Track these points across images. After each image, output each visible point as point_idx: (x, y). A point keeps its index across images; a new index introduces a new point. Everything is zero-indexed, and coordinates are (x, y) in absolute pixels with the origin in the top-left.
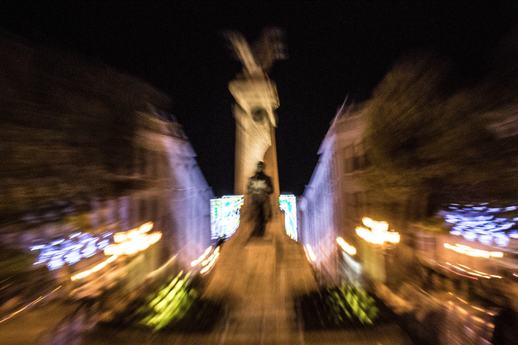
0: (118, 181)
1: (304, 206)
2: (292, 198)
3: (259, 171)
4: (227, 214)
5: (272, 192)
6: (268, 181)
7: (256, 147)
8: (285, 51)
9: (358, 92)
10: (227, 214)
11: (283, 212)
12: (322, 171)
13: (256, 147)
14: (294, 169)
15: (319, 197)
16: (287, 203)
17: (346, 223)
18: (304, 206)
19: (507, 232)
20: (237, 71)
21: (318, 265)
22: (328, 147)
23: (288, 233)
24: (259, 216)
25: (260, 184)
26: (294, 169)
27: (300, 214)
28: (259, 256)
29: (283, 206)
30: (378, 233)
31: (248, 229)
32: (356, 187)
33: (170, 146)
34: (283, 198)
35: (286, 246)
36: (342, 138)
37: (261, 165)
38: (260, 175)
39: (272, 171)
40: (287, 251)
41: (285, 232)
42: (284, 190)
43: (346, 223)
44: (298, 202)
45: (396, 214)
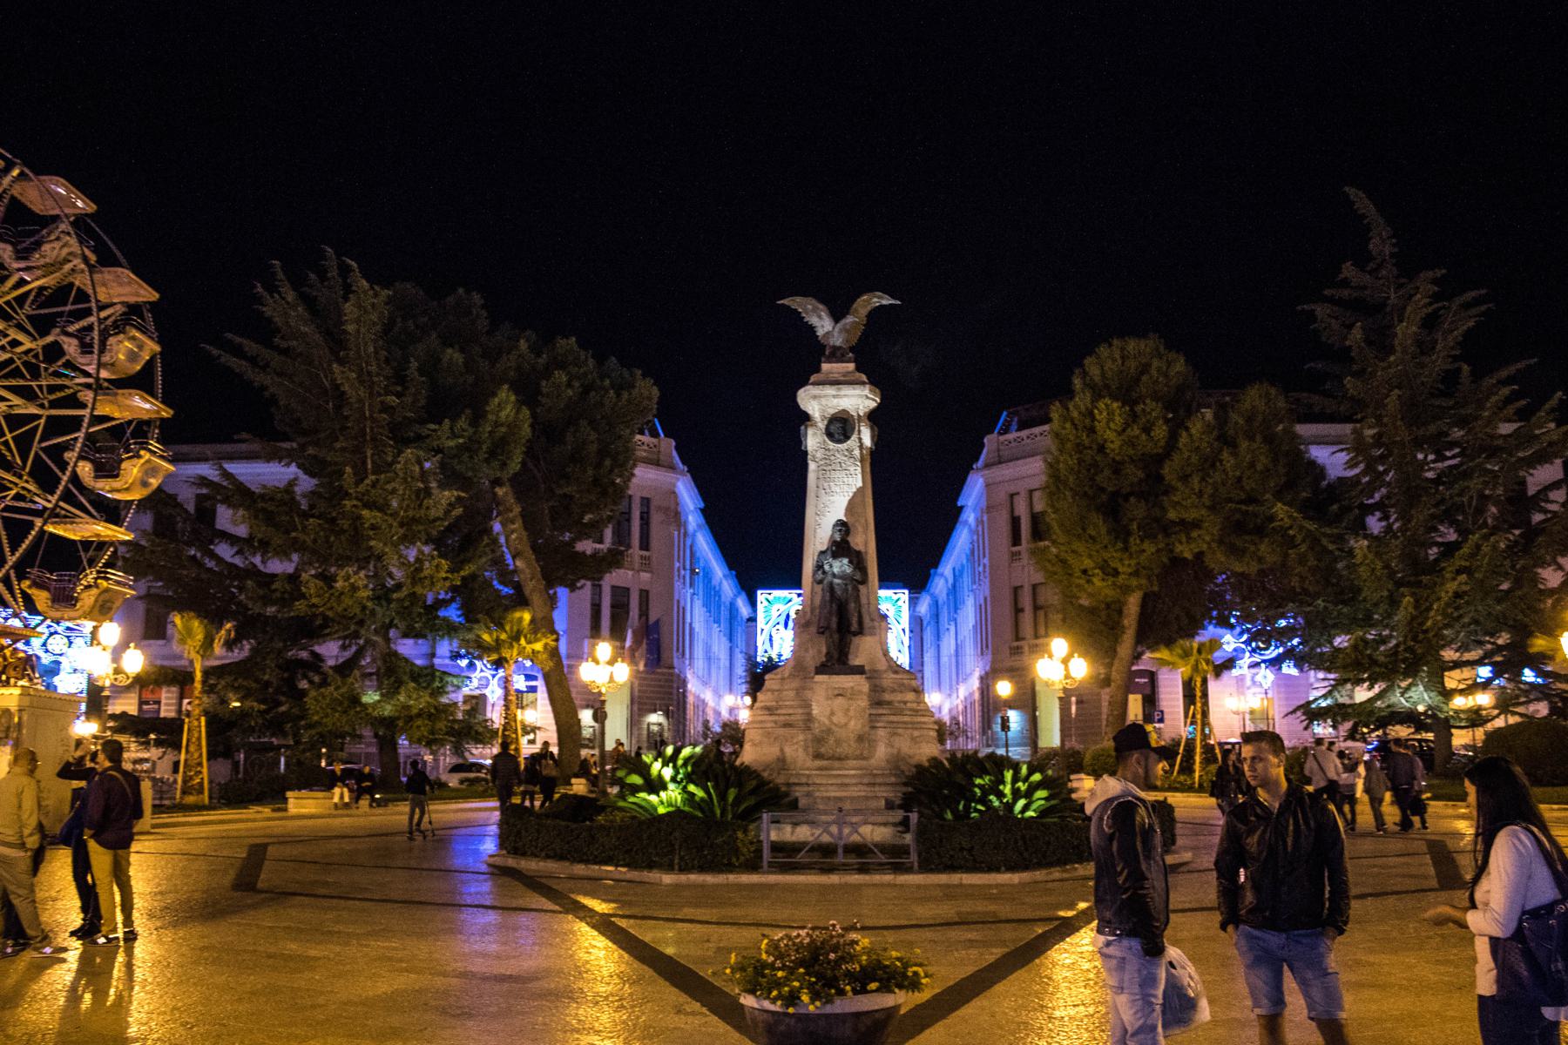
0: (574, 548)
1: (924, 608)
2: (904, 595)
3: (838, 537)
4: (777, 619)
5: (864, 581)
6: (858, 560)
7: (836, 492)
8: (877, 599)
9: (1032, 392)
10: (777, 619)
11: (885, 617)
12: (961, 541)
13: (836, 492)
14: (908, 537)
15: (954, 590)
16: (893, 603)
17: (1009, 646)
18: (924, 608)
19: (1275, 663)
20: (807, 359)
21: (946, 719)
22: (973, 493)
23: (893, 654)
24: (838, 628)
25: (840, 566)
26: (908, 537)
27: (917, 625)
28: (835, 704)
29: (884, 607)
30: (1061, 664)
31: (819, 650)
32: (1028, 573)
33: (665, 482)
34: (882, 593)
35: (888, 679)
36: (1005, 478)
37: (843, 527)
38: (840, 547)
39: (865, 540)
40: (892, 694)
41: (886, 653)
42: (887, 580)
43: (1009, 646)
44: (913, 602)
45: (1097, 630)
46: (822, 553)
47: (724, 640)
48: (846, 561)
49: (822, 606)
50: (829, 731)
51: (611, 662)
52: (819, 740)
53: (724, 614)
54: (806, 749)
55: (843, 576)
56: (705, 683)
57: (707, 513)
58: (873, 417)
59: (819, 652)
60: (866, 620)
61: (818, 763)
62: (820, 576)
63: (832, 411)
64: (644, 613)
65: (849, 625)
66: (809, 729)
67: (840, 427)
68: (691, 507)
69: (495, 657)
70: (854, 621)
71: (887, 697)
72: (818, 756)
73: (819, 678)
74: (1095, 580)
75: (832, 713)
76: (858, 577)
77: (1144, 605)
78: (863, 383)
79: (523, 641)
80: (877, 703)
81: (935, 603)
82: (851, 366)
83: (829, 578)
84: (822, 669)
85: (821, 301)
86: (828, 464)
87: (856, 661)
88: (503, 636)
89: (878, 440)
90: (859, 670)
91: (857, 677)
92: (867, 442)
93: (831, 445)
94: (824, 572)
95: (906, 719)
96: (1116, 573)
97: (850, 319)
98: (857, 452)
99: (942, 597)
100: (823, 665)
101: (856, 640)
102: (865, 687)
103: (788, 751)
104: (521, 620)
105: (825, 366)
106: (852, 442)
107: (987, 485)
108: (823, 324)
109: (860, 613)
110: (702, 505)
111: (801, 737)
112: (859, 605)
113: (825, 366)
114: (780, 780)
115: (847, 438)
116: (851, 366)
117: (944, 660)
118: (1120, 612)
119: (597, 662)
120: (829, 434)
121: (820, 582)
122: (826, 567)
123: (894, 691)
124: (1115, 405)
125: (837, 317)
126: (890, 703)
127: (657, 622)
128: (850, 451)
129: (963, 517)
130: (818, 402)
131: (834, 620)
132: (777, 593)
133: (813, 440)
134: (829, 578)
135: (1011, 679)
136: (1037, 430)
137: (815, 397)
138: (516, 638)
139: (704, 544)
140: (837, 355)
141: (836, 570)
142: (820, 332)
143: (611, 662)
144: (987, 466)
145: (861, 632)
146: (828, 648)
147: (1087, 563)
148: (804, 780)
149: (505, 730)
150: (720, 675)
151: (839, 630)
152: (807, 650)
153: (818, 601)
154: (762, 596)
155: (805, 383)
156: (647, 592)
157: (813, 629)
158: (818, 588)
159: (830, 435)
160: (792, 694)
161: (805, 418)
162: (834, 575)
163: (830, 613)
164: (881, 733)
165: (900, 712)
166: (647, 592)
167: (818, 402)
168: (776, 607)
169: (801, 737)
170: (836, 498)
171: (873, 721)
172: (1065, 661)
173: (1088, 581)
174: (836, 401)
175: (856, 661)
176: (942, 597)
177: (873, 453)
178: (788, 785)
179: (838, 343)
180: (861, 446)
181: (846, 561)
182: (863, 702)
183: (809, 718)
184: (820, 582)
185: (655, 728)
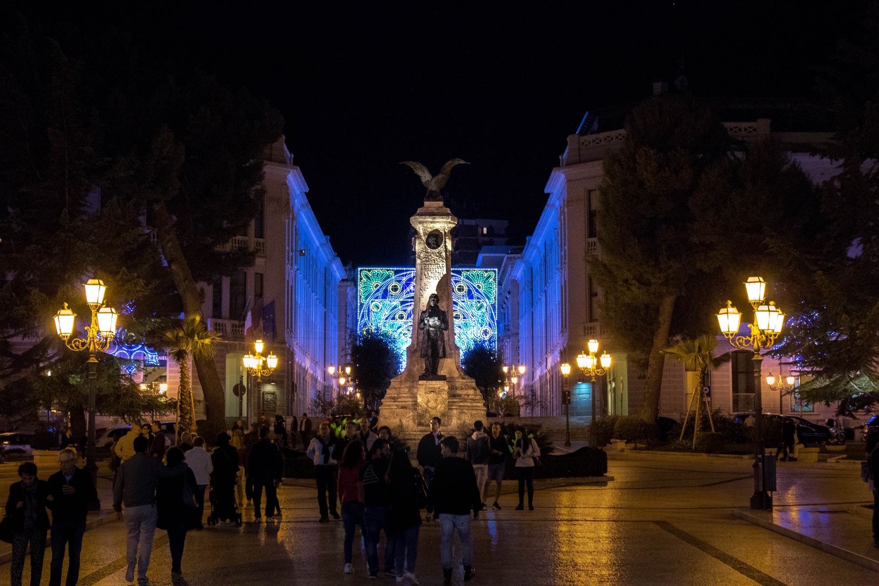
18: (519, 272)
20: (414, 199)
22: (558, 183)
25: (433, 321)
31: (421, 366)
46: (424, 312)
47: (321, 309)
48: (436, 318)
49: (423, 343)
50: (426, 411)
51: (265, 354)
52: (421, 416)
53: (320, 278)
54: (414, 420)
55: (435, 327)
56: (305, 353)
57: (314, 199)
58: (453, 233)
59: (422, 367)
60: (447, 349)
61: (420, 428)
62: (422, 325)
63: (430, 230)
64: (259, 295)
65: (438, 353)
66: (416, 409)
67: (435, 239)
68: (298, 193)
69: (176, 350)
70: (441, 351)
71: (458, 392)
72: (420, 424)
73: (421, 382)
74: (633, 288)
75: (428, 401)
76: (443, 326)
77: (677, 306)
78: (447, 215)
79: (196, 338)
80: (453, 396)
81: (531, 271)
82: (441, 203)
83: (427, 327)
84: (423, 377)
85: (425, 165)
86: (427, 261)
87: (442, 372)
88: (181, 334)
89: (455, 247)
90: (443, 378)
91: (442, 382)
92: (450, 248)
93: (429, 250)
94: (425, 324)
95: (469, 404)
96: (648, 284)
97: (440, 176)
98: (444, 254)
99: (537, 266)
100: (423, 375)
101: (441, 360)
102: (446, 388)
103: (404, 421)
104: (194, 320)
105: (426, 203)
106: (441, 248)
107: (569, 181)
108: (425, 176)
109: (444, 348)
110: (307, 190)
111: (411, 413)
112: (443, 341)
113: (426, 203)
114: (401, 437)
115: (438, 246)
116: (441, 203)
117: (537, 328)
118: (657, 310)
119: (254, 355)
120: (428, 244)
121: (423, 329)
122: (426, 322)
123: (462, 389)
124: (652, 152)
125: (434, 174)
126: (459, 395)
127: (273, 302)
128: (440, 253)
129: (551, 201)
130: (424, 225)
131: (430, 351)
132: (377, 270)
133: (419, 247)
134: (427, 327)
135: (559, 371)
136: (614, 133)
137: (420, 223)
138: (190, 335)
139: (305, 219)
140: (433, 197)
141: (431, 323)
142: (424, 180)
143: (265, 354)
144: (569, 164)
145: (444, 356)
146: (426, 365)
147: (627, 275)
148: (412, 437)
149: (182, 403)
150: (317, 344)
151: (433, 355)
152: (414, 366)
153: (421, 338)
154: (362, 272)
155: (413, 213)
156: (262, 275)
157: (418, 354)
158: (421, 332)
159: (428, 244)
160: (407, 390)
161: (416, 232)
162: (430, 326)
163: (427, 346)
164: (455, 412)
165: (465, 401)
166: (262, 275)
167: (424, 225)
168: (374, 283)
169: (411, 413)
170: (431, 280)
171: (450, 406)
172: (598, 355)
173: (629, 289)
174: (432, 225)
175: (442, 372)
176: (537, 266)
177: (452, 254)
178: (405, 440)
179: (434, 189)
180: (446, 251)
181: (436, 318)
182: (445, 396)
183: (416, 404)
184: (423, 329)
185: (270, 397)
